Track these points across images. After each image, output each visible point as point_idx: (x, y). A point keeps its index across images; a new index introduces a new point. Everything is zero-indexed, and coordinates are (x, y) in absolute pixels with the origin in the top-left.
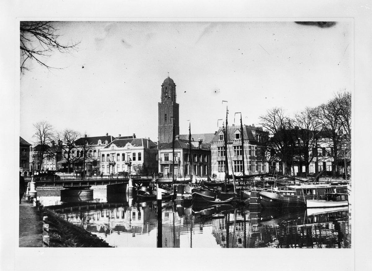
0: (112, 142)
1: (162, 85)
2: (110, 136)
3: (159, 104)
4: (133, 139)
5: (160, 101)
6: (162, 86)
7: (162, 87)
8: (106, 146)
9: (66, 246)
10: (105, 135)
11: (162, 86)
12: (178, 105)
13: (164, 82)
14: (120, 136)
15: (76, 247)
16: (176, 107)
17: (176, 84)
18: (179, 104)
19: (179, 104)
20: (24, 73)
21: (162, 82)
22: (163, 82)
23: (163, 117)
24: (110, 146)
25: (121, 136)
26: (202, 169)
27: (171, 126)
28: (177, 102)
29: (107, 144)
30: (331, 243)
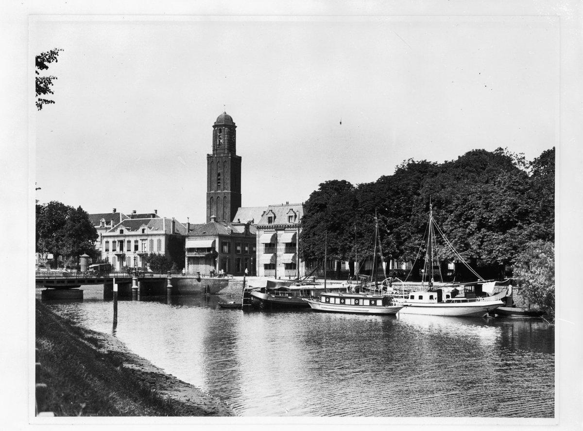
0: (121, 222)
1: (213, 124)
2: (119, 214)
3: (209, 157)
4: (150, 220)
5: (211, 152)
6: (214, 127)
7: (213, 129)
8: (112, 228)
9: (493, 411)
10: (112, 212)
11: (214, 127)
12: (239, 159)
13: (217, 120)
14: (135, 212)
15: (81, 416)
16: (236, 162)
17: (236, 125)
18: (241, 157)
19: (241, 157)
20: (396, 167)
21: (214, 120)
22: (215, 121)
23: (215, 178)
24: (117, 229)
25: (137, 213)
26: (219, 266)
27: (228, 193)
28: (238, 153)
29: (113, 226)
30: (545, 415)
